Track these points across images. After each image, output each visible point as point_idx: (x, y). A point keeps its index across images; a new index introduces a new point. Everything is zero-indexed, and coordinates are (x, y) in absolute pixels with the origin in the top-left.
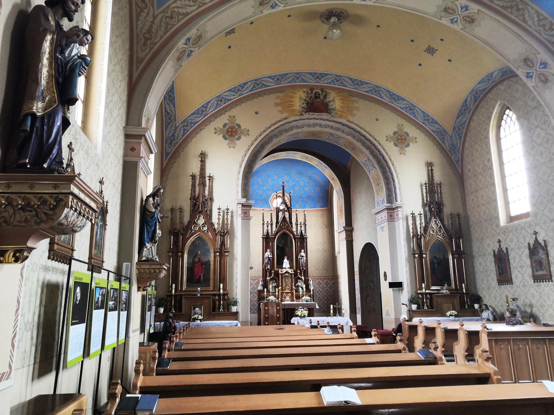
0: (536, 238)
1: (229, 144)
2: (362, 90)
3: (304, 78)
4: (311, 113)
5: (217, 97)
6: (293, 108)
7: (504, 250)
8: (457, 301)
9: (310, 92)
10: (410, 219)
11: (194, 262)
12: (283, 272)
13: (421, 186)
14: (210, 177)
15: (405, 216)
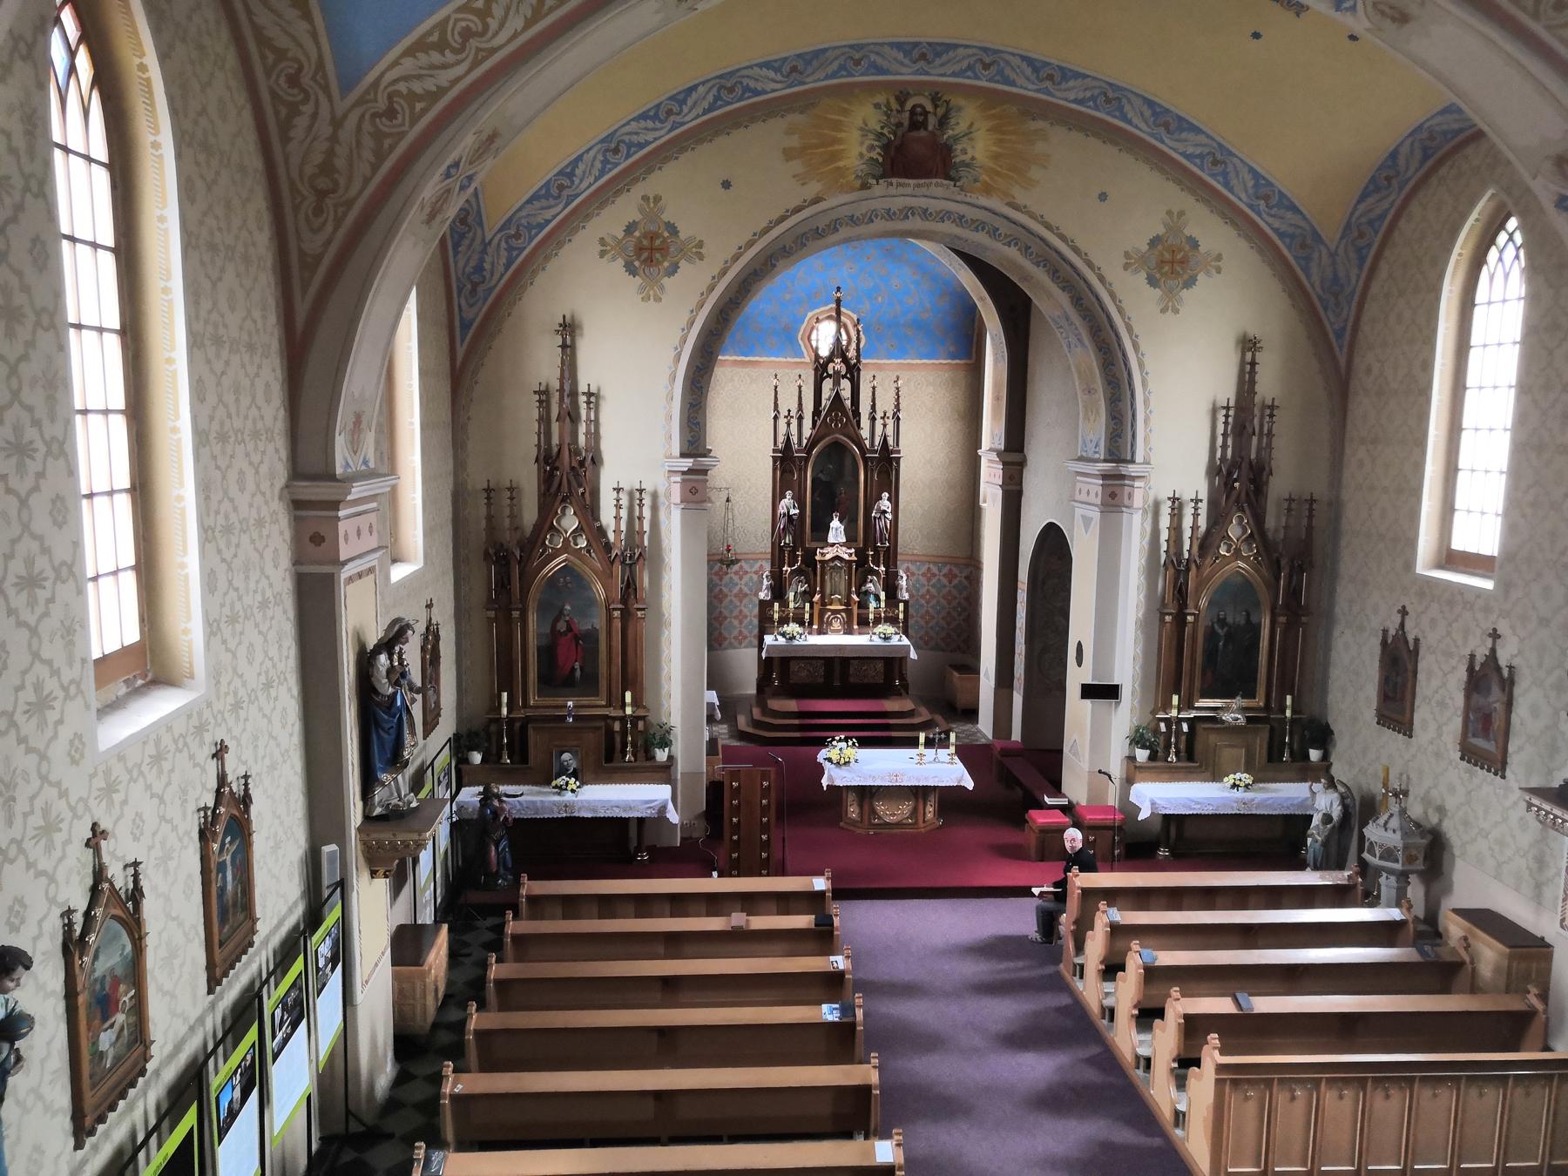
0: (1493, 650)
1: (642, 289)
2: (1065, 97)
3: (879, 60)
4: (894, 181)
5: (602, 141)
6: (841, 164)
7: (1411, 638)
8: (1260, 742)
9: (895, 105)
10: (1166, 510)
11: (554, 632)
12: (828, 557)
13: (1214, 411)
14: (589, 394)
15: (1151, 501)
